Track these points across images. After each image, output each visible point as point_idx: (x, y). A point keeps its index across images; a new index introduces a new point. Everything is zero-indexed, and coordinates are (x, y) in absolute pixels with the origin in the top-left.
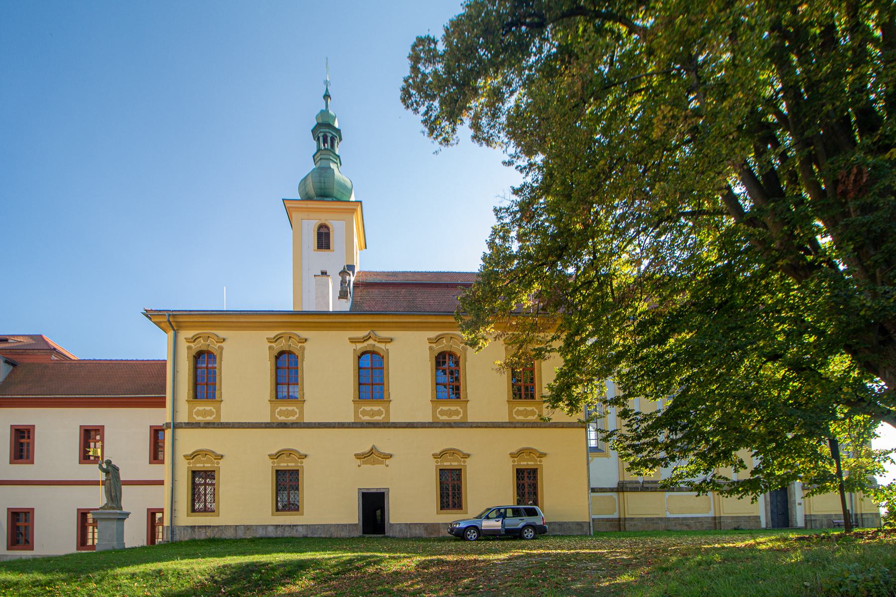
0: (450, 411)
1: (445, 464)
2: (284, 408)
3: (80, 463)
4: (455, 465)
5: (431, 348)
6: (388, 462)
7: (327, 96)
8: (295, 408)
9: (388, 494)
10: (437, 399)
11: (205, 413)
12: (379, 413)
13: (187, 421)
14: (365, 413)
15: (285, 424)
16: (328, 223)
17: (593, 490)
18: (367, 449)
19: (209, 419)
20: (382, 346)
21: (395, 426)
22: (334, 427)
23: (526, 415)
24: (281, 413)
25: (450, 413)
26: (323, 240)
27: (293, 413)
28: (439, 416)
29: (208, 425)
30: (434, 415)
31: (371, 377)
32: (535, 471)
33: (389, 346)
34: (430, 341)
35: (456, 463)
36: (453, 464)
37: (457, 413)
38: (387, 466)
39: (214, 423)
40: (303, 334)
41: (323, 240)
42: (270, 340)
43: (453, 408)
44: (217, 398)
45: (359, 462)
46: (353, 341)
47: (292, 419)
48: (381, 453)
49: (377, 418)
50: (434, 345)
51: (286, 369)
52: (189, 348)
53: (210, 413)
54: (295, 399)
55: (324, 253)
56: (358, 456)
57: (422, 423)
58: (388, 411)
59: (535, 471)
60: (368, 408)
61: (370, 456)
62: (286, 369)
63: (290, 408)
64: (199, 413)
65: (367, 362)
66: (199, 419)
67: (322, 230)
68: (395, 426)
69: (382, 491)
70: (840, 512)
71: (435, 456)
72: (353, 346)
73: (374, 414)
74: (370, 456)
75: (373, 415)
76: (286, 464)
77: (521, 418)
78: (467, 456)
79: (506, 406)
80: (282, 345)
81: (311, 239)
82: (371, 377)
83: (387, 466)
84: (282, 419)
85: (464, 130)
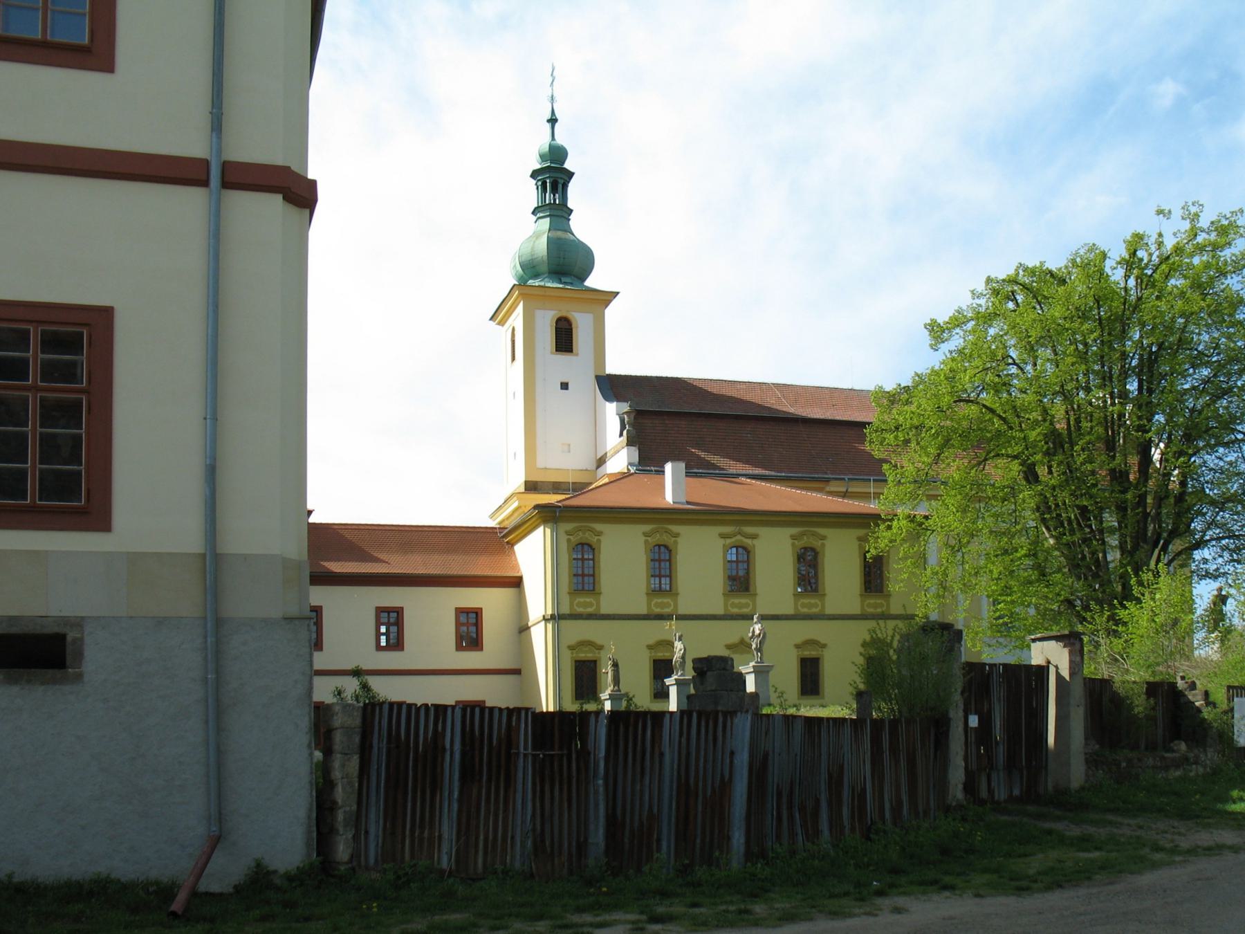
0: (810, 604)
3: (482, 649)
5: (793, 545)
7: (553, 121)
11: (586, 605)
17: (517, 672)
20: (749, 541)
23: (876, 607)
24: (657, 605)
25: (810, 606)
26: (564, 339)
29: (590, 617)
33: (755, 542)
34: (793, 537)
37: (816, 606)
41: (564, 339)
42: (645, 534)
43: (813, 601)
46: (723, 536)
47: (815, 610)
51: (662, 562)
52: (569, 540)
54: (671, 592)
55: (563, 358)
58: (888, 605)
60: (736, 601)
62: (662, 562)
64: (579, 605)
66: (580, 610)
70: (190, 540)
71: (797, 646)
77: (871, 610)
78: (824, 646)
79: (859, 599)
80: (657, 539)
81: (547, 337)
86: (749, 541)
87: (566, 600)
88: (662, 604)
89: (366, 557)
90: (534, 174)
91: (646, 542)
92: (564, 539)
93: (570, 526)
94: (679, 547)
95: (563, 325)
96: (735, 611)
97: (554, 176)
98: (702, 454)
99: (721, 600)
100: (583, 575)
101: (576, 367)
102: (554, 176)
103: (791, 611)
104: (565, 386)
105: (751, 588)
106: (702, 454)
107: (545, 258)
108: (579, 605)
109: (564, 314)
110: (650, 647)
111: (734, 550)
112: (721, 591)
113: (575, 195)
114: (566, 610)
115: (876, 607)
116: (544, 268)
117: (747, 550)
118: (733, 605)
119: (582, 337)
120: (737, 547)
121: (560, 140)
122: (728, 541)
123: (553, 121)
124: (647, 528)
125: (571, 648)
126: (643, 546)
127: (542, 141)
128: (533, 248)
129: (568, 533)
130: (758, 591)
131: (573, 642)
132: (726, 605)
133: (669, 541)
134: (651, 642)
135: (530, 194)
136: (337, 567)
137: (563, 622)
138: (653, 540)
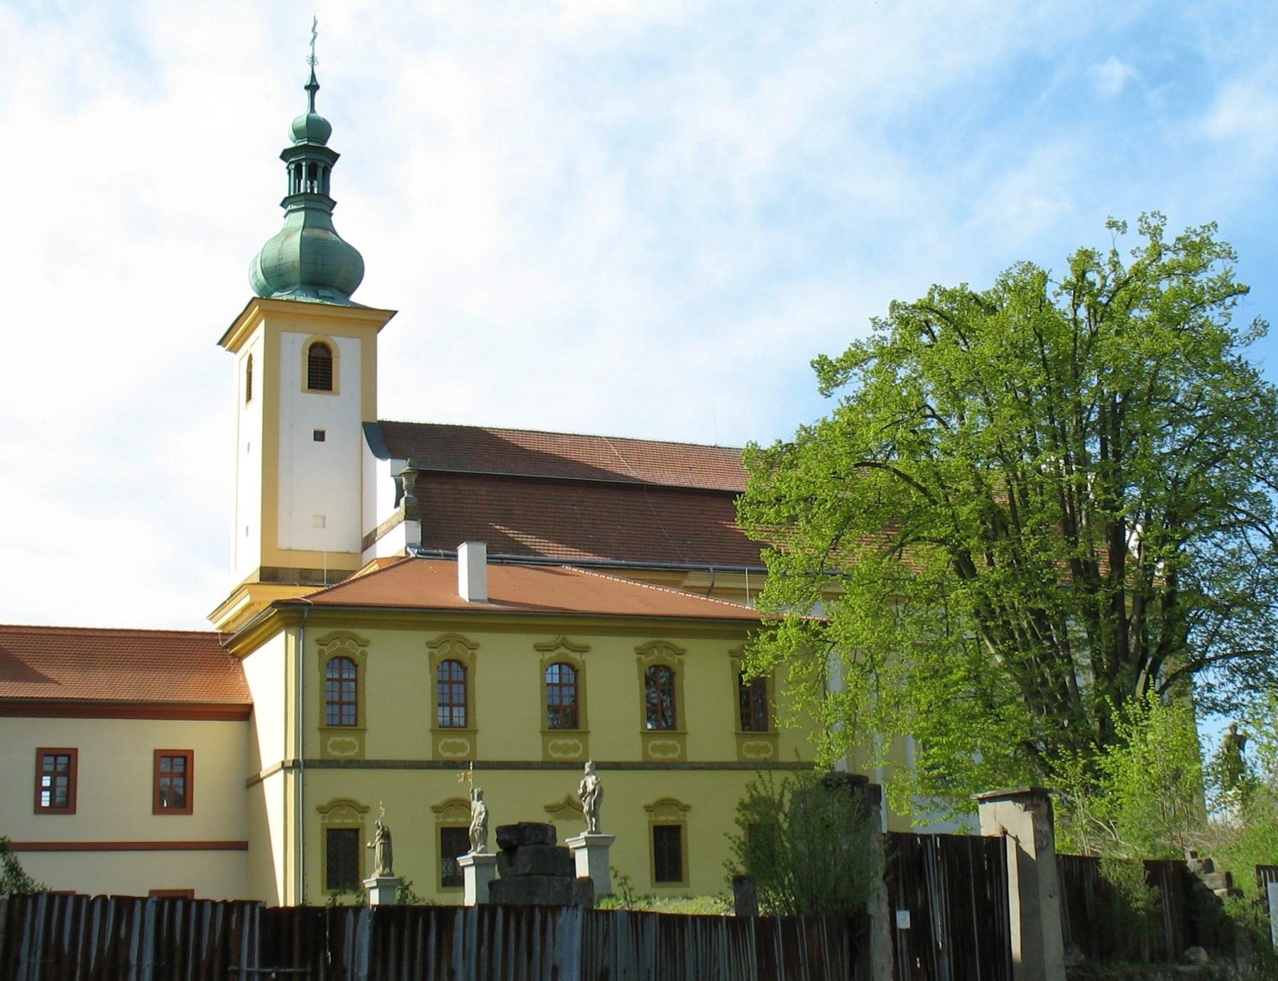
0: (665, 748)
2: (450, 741)
4: (349, 822)
5: (639, 661)
8: (353, 739)
14: (556, 748)
15: (454, 762)
20: (576, 656)
26: (320, 372)
28: (329, 750)
30: (645, 753)
32: (356, 831)
33: (585, 656)
34: (639, 651)
35: (350, 821)
40: (472, 637)
41: (320, 372)
42: (431, 645)
44: (679, 730)
46: (540, 648)
52: (321, 653)
54: (467, 728)
55: (318, 398)
57: (393, 761)
58: (776, 748)
59: (356, 831)
62: (453, 684)
66: (336, 754)
72: (539, 656)
75: (566, 752)
76: (344, 821)
79: (539, 739)
81: (296, 367)
84: (448, 755)
86: (576, 656)
87: (315, 737)
89: (25, 674)
91: (431, 656)
92: (314, 649)
93: (322, 632)
95: (321, 353)
97: (311, 157)
98: (511, 533)
102: (311, 157)
103: (537, 757)
104: (319, 436)
106: (511, 533)
107: (297, 264)
109: (321, 338)
110: (436, 809)
111: (556, 668)
116: (296, 277)
120: (560, 664)
121: (321, 112)
122: (548, 655)
123: (313, 88)
127: (298, 112)
128: (280, 250)
129: (320, 642)
130: (369, 726)
134: (438, 801)
135: (279, 180)
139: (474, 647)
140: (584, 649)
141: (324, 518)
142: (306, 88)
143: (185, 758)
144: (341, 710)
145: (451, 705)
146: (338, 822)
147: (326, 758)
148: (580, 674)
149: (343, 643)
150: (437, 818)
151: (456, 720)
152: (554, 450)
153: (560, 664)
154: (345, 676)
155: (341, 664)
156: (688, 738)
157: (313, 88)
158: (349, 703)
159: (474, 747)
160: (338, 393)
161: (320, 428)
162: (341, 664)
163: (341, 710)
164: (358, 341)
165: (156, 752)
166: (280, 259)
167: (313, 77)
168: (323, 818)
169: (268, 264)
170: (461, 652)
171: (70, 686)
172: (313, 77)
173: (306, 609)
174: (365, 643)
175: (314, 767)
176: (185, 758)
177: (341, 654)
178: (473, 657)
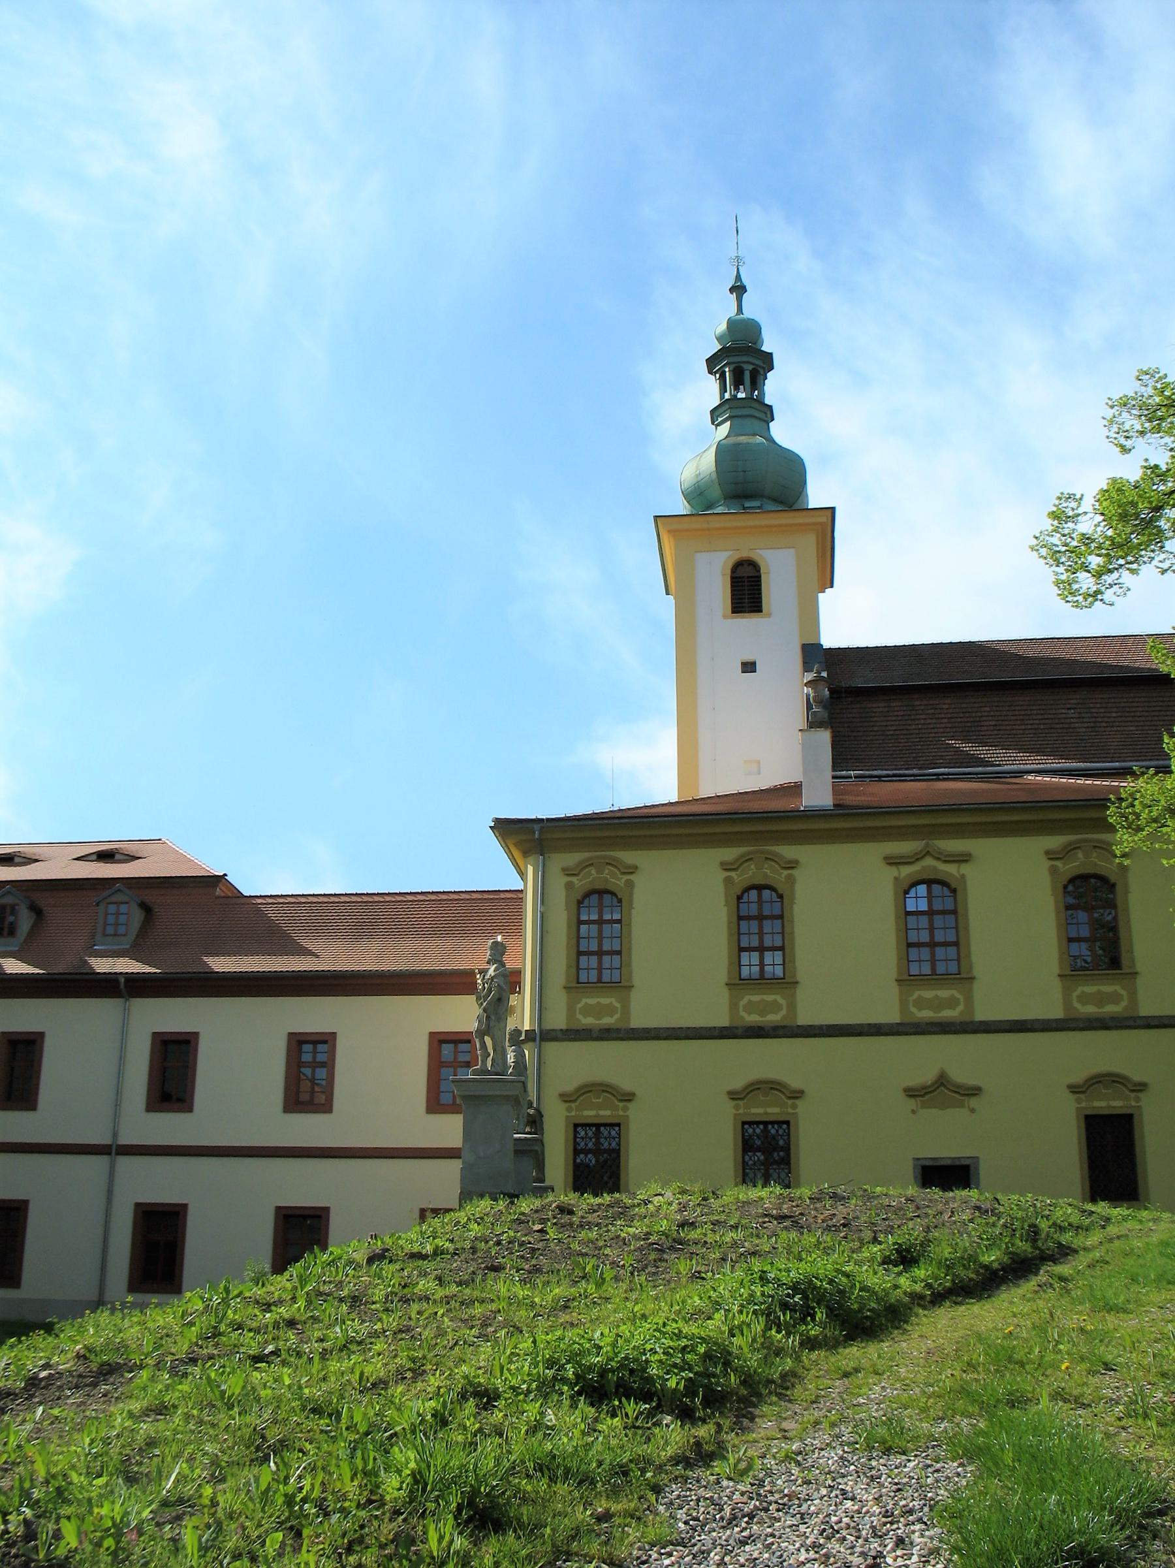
0: (1099, 995)
1: (754, 1111)
2: (756, 998)
4: (773, 1112)
5: (1053, 871)
6: (973, 1102)
9: (977, 1168)
10: (1075, 970)
11: (600, 1011)
12: (952, 1003)
13: (564, 1027)
14: (921, 1004)
15: (761, 1028)
16: (755, 556)
18: (927, 1076)
19: (608, 1021)
20: (952, 869)
21: (987, 1028)
22: (860, 1034)
25: (1101, 999)
26: (746, 592)
27: (775, 1007)
31: (934, 938)
33: (965, 869)
34: (1051, 855)
35: (608, 1113)
36: (602, 1113)
37: (1115, 998)
38: (973, 1111)
39: (618, 1030)
40: (788, 851)
41: (746, 592)
42: (726, 866)
43: (1107, 989)
45: (912, 1103)
46: (893, 861)
47: (774, 1018)
48: (959, 1086)
49: (948, 1014)
50: (1059, 864)
51: (760, 915)
52: (569, 886)
53: (610, 1010)
55: (747, 622)
56: (912, 1093)
58: (969, 1000)
60: (1090, 989)
61: (940, 1092)
62: (760, 915)
63: (769, 998)
64: (587, 1011)
65: (918, 901)
66: (588, 1021)
67: (741, 572)
68: (987, 1028)
69: (967, 1162)
71: (1075, 1089)
72: (893, 872)
73: (939, 1004)
74: (940, 1092)
76: (1108, 1103)
80: (750, 874)
81: (715, 589)
82: (934, 938)
83: (973, 1111)
84: (753, 1019)
85: (1110, 413)
86: (951, 870)
87: (558, 1001)
88: (598, 1009)
89: (286, 945)
90: (711, 362)
91: (728, 881)
92: (558, 884)
93: (572, 859)
94: (798, 888)
95: (746, 571)
96: (926, 1014)
97: (742, 361)
98: (966, 747)
99: (1055, 988)
100: (600, 953)
101: (770, 637)
102: (742, 361)
103: (892, 1016)
104: (749, 667)
105: (1125, 961)
106: (966, 747)
107: (714, 476)
108: (587, 1011)
109: (745, 554)
110: (734, 1096)
112: (1055, 969)
113: (773, 388)
114: (558, 1020)
115: (762, 1013)
116: (716, 492)
117: (951, 888)
118: (921, 1004)
119: (779, 584)
120: (929, 882)
121: (751, 311)
122: (906, 871)
123: (739, 289)
124: (730, 853)
125: (566, 1098)
126: (721, 888)
127: (721, 312)
128: (697, 468)
129: (568, 872)
130: (1139, 967)
131: (569, 1087)
132: (904, 1004)
133: (777, 877)
134: (738, 1084)
135: (709, 391)
136: (221, 964)
137: (551, 1048)
138: (741, 878)
139: (792, 865)
140: (963, 858)
141: (759, 762)
142: (732, 290)
143: (442, 1042)
144: (600, 963)
145: (761, 949)
146: (589, 1115)
147: (574, 1027)
148: (959, 893)
149: (599, 871)
150: (1078, 1101)
151: (768, 969)
152: (1048, 653)
153: (929, 882)
154: (607, 917)
155: (601, 899)
156: (1140, 981)
157: (739, 289)
158: (589, 953)
159: (792, 1006)
160: (769, 615)
161: (749, 658)
162: (601, 899)
163: (600, 963)
164: (792, 551)
165: (432, 1035)
166: (697, 476)
167: (738, 277)
168: (569, 1110)
169: (686, 485)
170: (772, 874)
171: (331, 956)
172: (738, 277)
173: (537, 827)
174: (632, 870)
175: (555, 1039)
176: (442, 1042)
177: (599, 886)
178: (791, 880)
